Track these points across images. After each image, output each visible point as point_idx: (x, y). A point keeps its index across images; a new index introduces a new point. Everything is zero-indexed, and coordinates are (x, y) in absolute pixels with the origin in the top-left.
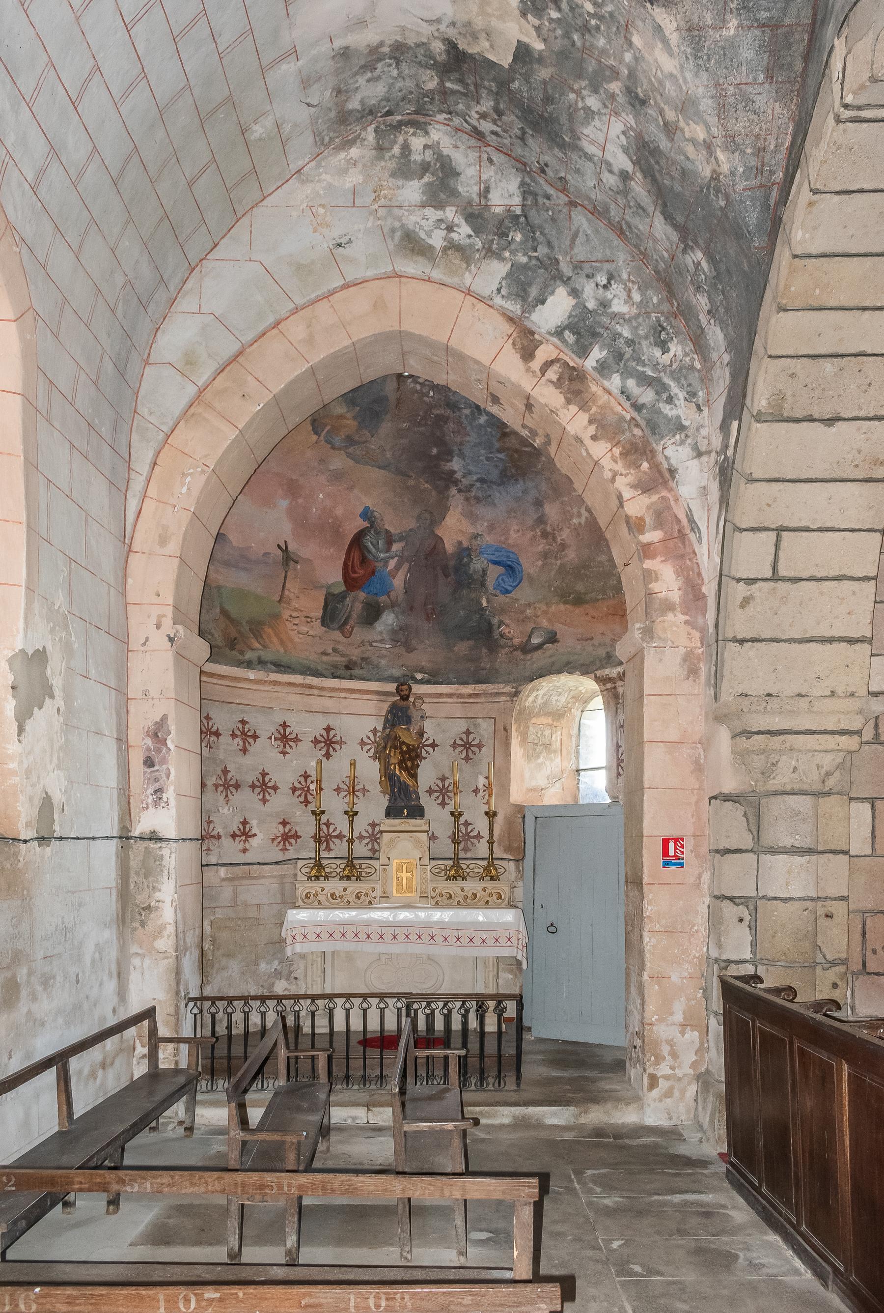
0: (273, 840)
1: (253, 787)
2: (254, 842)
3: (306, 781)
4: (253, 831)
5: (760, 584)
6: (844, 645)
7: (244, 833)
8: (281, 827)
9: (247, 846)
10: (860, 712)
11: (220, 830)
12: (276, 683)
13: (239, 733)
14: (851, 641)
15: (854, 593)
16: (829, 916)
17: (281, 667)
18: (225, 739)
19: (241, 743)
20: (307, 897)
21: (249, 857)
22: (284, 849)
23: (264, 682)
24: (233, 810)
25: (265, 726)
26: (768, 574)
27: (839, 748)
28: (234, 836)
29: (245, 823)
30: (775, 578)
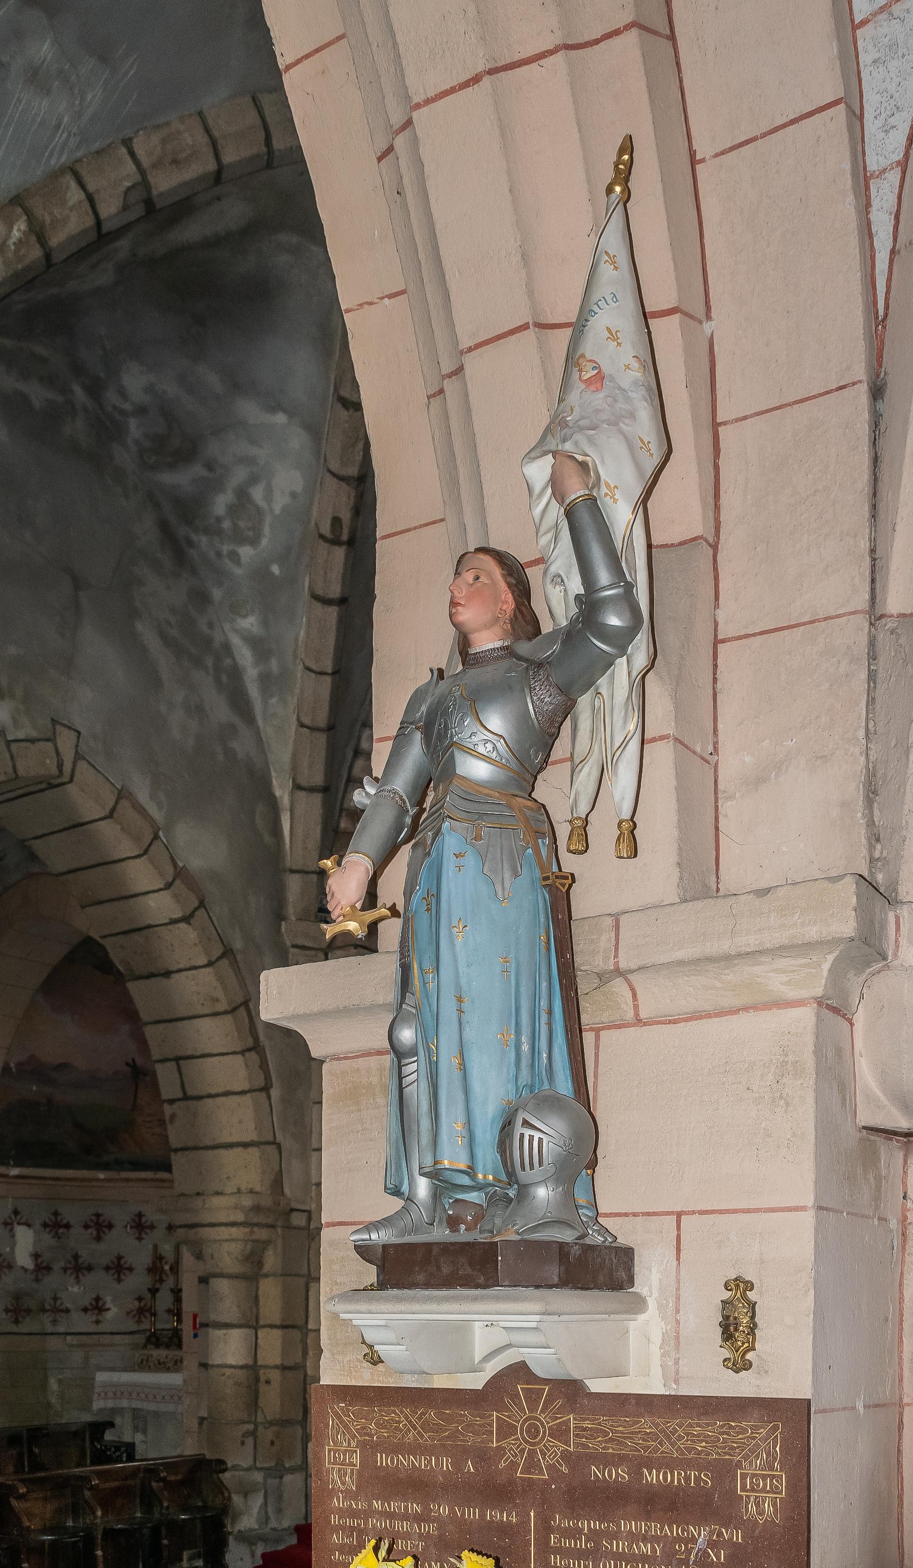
0: (128, 1313)
1: (107, 1268)
2: (109, 1315)
3: (160, 1263)
4: (107, 1306)
5: (178, 1103)
6: (240, 1149)
7: (97, 1307)
8: (136, 1303)
9: (100, 1318)
10: (236, 1207)
11: (68, 1305)
12: (128, 1180)
13: (92, 1224)
14: (245, 1145)
15: (239, 1105)
16: (268, 1382)
17: (137, 1165)
18: (77, 1231)
19: (95, 1232)
20: (142, 1362)
21: (101, 1328)
22: (17, 1322)
23: (117, 1180)
24: (84, 1289)
25: (120, 1217)
26: (180, 1095)
27: (231, 1238)
28: (85, 1310)
29: (98, 1299)
30: (186, 1098)
